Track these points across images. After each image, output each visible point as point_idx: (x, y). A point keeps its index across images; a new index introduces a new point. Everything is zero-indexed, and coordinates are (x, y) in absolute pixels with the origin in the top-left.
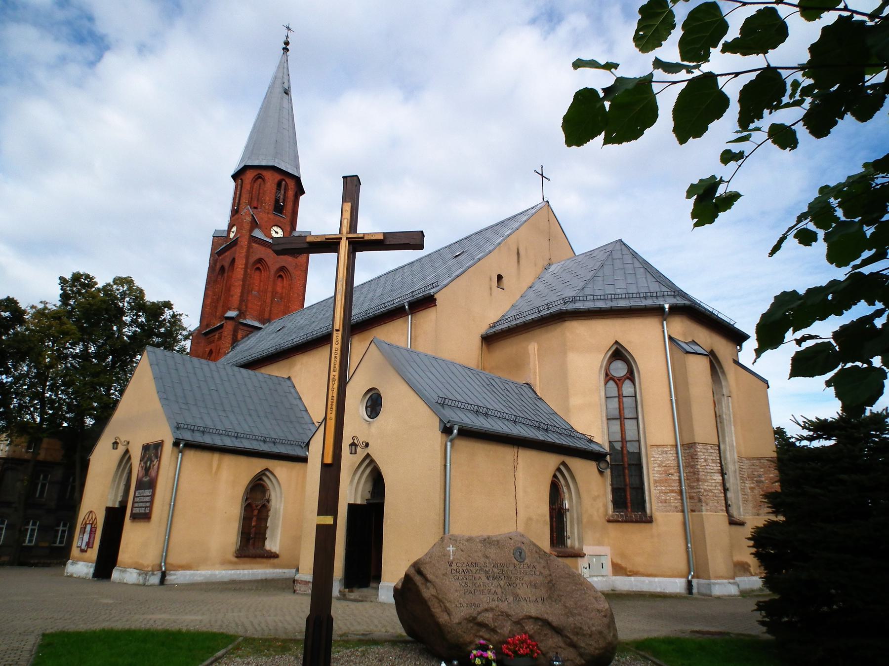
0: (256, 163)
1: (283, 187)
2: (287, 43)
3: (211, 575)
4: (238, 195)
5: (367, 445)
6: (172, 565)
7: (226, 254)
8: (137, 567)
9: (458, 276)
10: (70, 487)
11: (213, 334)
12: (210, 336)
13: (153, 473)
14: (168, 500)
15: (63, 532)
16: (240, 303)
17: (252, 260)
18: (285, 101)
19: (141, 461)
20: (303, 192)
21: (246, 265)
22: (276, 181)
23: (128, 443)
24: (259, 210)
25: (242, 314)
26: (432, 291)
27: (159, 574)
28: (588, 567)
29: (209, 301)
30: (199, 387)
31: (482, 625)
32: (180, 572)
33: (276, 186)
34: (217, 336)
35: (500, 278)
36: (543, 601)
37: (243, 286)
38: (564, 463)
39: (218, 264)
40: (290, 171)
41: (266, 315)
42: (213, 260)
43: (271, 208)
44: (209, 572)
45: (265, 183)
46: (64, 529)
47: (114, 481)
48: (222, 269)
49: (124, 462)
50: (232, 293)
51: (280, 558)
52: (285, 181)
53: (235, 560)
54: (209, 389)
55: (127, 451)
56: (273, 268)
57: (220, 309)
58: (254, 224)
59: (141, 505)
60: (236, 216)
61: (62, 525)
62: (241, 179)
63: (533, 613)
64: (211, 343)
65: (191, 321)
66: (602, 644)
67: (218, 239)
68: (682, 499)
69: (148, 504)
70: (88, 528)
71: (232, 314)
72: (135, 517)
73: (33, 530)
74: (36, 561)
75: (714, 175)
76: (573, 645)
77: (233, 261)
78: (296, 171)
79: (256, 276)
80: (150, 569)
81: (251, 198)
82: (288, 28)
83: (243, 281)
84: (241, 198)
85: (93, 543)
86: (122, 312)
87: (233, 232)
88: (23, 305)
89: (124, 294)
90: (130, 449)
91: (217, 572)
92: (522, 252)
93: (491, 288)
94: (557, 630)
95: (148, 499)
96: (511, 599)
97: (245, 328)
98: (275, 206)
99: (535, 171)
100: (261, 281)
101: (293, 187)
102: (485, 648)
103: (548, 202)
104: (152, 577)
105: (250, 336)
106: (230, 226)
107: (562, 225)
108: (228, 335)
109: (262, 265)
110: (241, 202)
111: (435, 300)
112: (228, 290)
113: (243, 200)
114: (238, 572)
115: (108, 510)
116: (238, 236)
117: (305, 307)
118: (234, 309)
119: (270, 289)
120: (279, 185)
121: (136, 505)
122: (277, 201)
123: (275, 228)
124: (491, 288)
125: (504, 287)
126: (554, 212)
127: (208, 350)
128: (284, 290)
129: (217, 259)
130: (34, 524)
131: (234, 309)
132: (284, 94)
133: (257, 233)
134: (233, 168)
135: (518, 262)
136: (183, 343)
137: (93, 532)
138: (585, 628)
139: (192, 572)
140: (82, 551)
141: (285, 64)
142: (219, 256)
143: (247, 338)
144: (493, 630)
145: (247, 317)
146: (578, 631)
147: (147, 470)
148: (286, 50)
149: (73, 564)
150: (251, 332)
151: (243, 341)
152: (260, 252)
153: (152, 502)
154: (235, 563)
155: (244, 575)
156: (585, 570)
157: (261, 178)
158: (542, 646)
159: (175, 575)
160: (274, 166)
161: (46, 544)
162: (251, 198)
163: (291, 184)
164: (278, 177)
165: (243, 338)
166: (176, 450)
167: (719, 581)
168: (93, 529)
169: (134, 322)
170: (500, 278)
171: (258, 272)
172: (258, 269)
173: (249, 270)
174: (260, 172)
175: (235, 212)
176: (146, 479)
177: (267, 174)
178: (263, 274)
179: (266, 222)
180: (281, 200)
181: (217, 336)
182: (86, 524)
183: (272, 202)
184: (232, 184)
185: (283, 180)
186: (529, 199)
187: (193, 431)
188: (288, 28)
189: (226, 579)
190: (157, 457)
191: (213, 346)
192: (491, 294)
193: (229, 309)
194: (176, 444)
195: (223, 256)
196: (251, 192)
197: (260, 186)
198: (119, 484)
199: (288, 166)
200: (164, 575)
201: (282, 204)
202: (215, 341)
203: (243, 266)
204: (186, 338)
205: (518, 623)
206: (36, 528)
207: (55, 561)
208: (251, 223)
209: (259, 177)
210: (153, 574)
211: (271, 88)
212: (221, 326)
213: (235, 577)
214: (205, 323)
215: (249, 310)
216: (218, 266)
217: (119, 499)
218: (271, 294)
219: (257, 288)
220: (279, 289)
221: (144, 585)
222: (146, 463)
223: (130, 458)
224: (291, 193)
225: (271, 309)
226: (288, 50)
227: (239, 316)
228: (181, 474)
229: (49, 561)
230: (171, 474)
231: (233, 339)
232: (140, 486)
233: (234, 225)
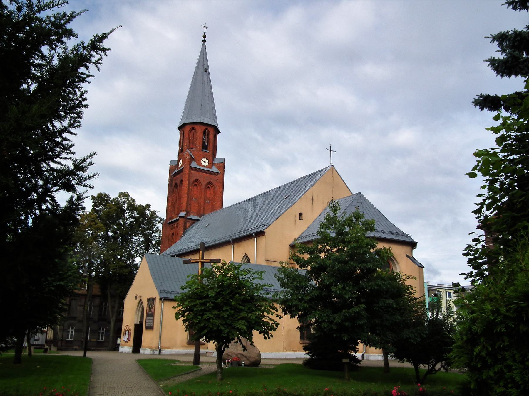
0: (191, 121)
1: (207, 134)
2: (205, 37)
3: (178, 351)
4: (182, 141)
6: (163, 347)
7: (178, 176)
8: (150, 348)
9: (277, 219)
10: (103, 309)
11: (174, 224)
12: (173, 224)
13: (153, 310)
14: (159, 322)
15: (103, 333)
16: (187, 207)
17: (192, 180)
18: (206, 77)
19: (147, 305)
20: (219, 132)
21: (189, 184)
22: (203, 130)
23: (141, 296)
24: (194, 149)
25: (188, 213)
26: (263, 229)
27: (158, 350)
29: (170, 204)
30: (168, 271)
31: (229, 355)
32: (166, 350)
33: (203, 134)
34: (175, 225)
35: (301, 214)
37: (188, 197)
39: (173, 181)
40: (210, 123)
41: (202, 212)
42: (171, 179)
43: (201, 147)
44: (177, 350)
45: (196, 133)
46: (103, 331)
47: (136, 313)
48: (176, 184)
50: (182, 202)
53: (187, 345)
54: (172, 272)
55: (141, 300)
56: (204, 184)
58: (192, 159)
59: (149, 323)
60: (181, 153)
62: (183, 130)
63: (240, 353)
64: (173, 228)
65: (162, 213)
66: (255, 359)
67: (173, 166)
69: (152, 323)
70: (127, 332)
71: (183, 214)
72: (147, 328)
73: (72, 332)
74: (94, 349)
75: (360, 193)
76: (248, 359)
77: (182, 181)
78: (214, 122)
79: (195, 189)
80: (155, 348)
81: (189, 142)
82: (205, 27)
83: (187, 194)
84: (184, 143)
85: (130, 339)
86: (124, 211)
87: (181, 163)
89: (124, 202)
90: (142, 299)
91: (180, 350)
92: (314, 198)
93: (295, 221)
94: (245, 357)
95: (151, 321)
96: (236, 350)
97: (190, 221)
98: (203, 146)
99: (326, 149)
100: (197, 192)
101: (212, 132)
102: (229, 360)
103: (333, 166)
104: (156, 351)
105: (193, 225)
106: (179, 159)
107: (342, 177)
108: (181, 226)
110: (184, 145)
112: (180, 198)
113: (185, 144)
114: (189, 350)
115: (136, 325)
116: (183, 167)
117: (224, 207)
119: (203, 197)
120: (204, 132)
121: (147, 323)
122: (204, 142)
123: (204, 160)
124: (295, 221)
125: (303, 219)
126: (337, 170)
127: (171, 232)
128: (211, 195)
129: (173, 179)
130: (72, 328)
132: (205, 72)
133: (194, 165)
134: (178, 124)
135: (312, 203)
136: (158, 225)
137: (129, 335)
139: (170, 350)
140: (126, 342)
141: (205, 52)
142: (174, 177)
143: (191, 227)
144: (231, 356)
145: (191, 214)
146: (250, 357)
147: (150, 309)
148: (204, 41)
149: (122, 347)
150: (194, 223)
151: (189, 228)
152: (196, 175)
153: (153, 322)
154: (187, 347)
155: (191, 351)
157: (194, 129)
158: (241, 360)
159: (164, 351)
161: (95, 340)
162: (189, 142)
163: (212, 131)
164: (204, 128)
165: (189, 227)
166: (161, 302)
167: (373, 354)
168: (130, 333)
169: (131, 216)
170: (301, 214)
171: (195, 186)
172: (196, 185)
173: (190, 187)
174: (193, 126)
175: (181, 151)
176: (150, 313)
177: (197, 127)
178: (198, 188)
179: (198, 157)
180: (206, 142)
181: (175, 225)
182: (126, 331)
183: (201, 144)
184: (178, 132)
185: (206, 129)
186: (322, 164)
187: (167, 293)
188: (205, 27)
189: (184, 353)
190: (154, 304)
191: (174, 230)
192: (295, 224)
193: (181, 211)
194: (161, 299)
195: (176, 177)
196: (189, 139)
197: (194, 134)
198: (138, 314)
199: (209, 120)
200: (160, 351)
201: (207, 144)
202: (175, 228)
203: (187, 186)
204: (159, 222)
205: (237, 355)
206: (74, 330)
207: (103, 349)
208: (190, 159)
209: (193, 129)
210: (156, 350)
211: (197, 68)
212: (177, 220)
213: (187, 352)
214: (169, 217)
215: (192, 210)
216: (174, 183)
217: (139, 320)
219: (196, 196)
220: (208, 195)
221: (153, 354)
222: (149, 306)
223: (142, 303)
224: (212, 136)
226: (206, 41)
227: (186, 215)
228: (164, 311)
229: (100, 348)
230: (160, 311)
231: (184, 228)
232: (148, 315)
233: (180, 159)
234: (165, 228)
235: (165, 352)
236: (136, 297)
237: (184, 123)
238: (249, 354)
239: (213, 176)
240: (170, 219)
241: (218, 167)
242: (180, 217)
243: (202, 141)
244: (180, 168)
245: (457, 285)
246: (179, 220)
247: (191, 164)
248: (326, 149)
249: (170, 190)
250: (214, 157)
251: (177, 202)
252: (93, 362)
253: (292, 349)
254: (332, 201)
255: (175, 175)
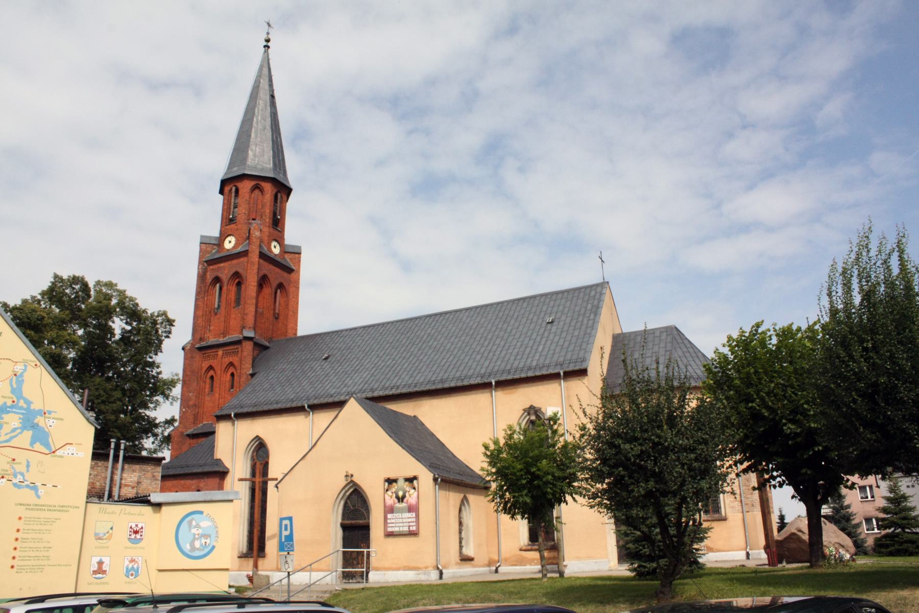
5: (352, 476)
7: (222, 265)
29: (200, 313)
51: (475, 560)
68: (742, 505)
82: (269, 25)
88: (64, 278)
118: (250, 328)
148: (267, 47)
188: (269, 25)
209: (256, 187)
216: (209, 277)
226: (268, 47)
234: (190, 355)
235: (721, 495)
249: (200, 287)
252: (844, 591)
254: (486, 448)
255: (211, 262)
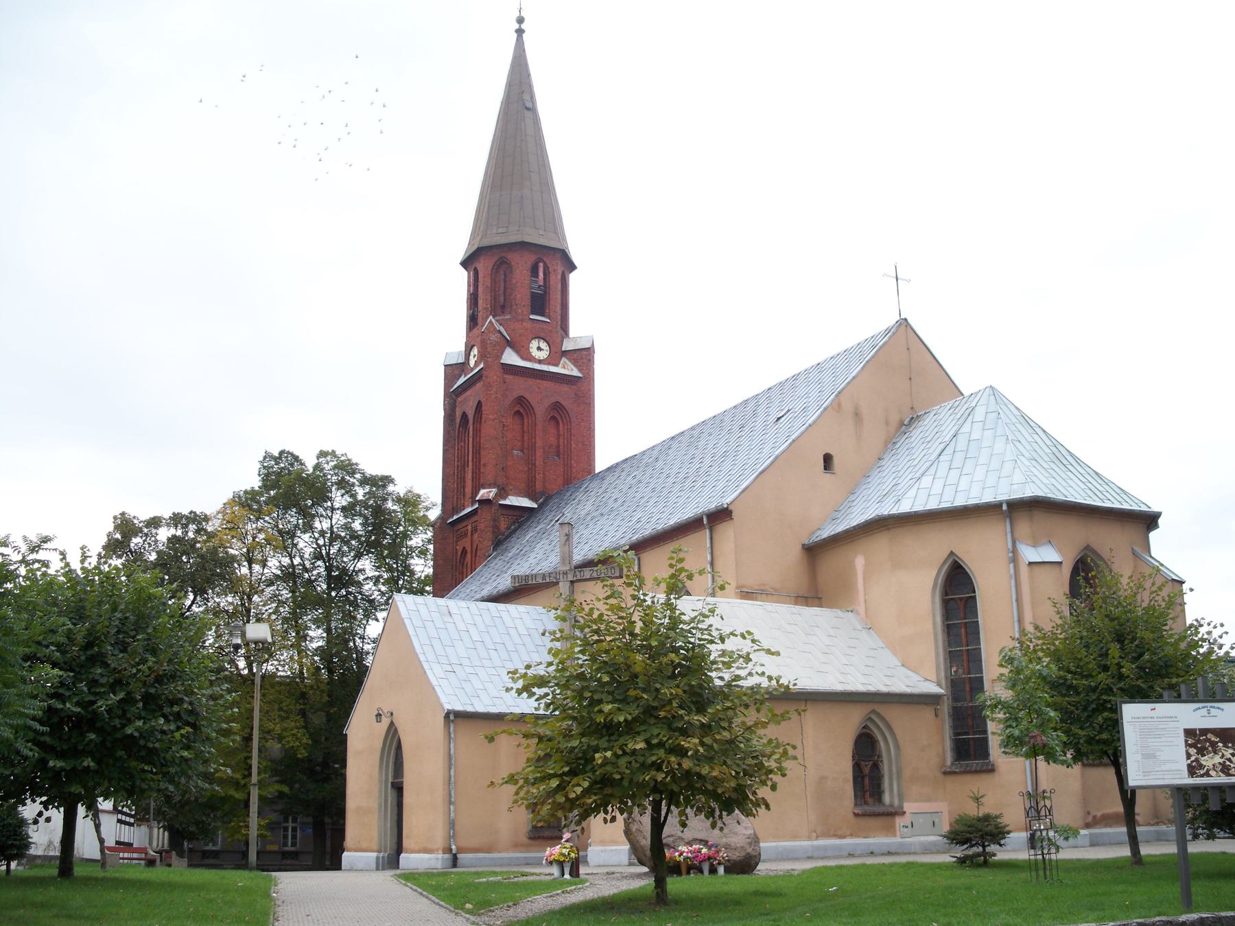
2: (520, 20)
7: (468, 393)
11: (464, 524)
12: (460, 526)
22: (529, 264)
23: (392, 714)
28: (910, 826)
33: (529, 273)
34: (469, 527)
35: (828, 460)
36: (707, 830)
38: (873, 711)
45: (511, 272)
49: (390, 736)
52: (545, 263)
53: (528, 841)
55: (392, 723)
57: (468, 490)
61: (290, 820)
66: (743, 854)
103: (906, 320)
109: (522, 406)
111: (731, 512)
131: (490, 486)
133: (510, 357)
134: (460, 254)
138: (733, 845)
148: (520, 32)
152: (520, 387)
156: (906, 830)
160: (523, 242)
170: (828, 460)
177: (514, 258)
178: (526, 421)
184: (463, 276)
218: (542, 450)
225: (544, 474)
233: (473, 346)
236: (379, 715)
237: (478, 248)
238: (724, 840)
239: (565, 388)
240: (456, 510)
241: (576, 363)
242: (480, 502)
243: (529, 294)
244: (472, 369)
245: (1066, 839)
246: (479, 511)
247: (503, 357)
248: (885, 275)
250: (564, 335)
251: (470, 463)
253: (832, 832)
